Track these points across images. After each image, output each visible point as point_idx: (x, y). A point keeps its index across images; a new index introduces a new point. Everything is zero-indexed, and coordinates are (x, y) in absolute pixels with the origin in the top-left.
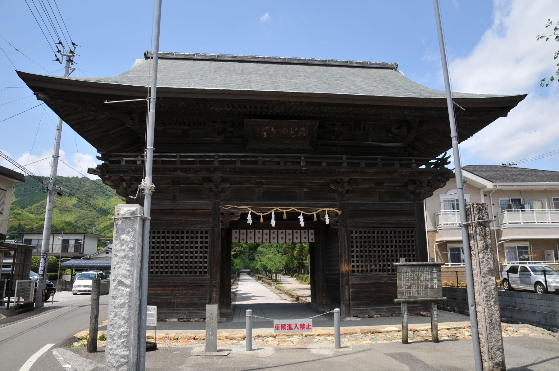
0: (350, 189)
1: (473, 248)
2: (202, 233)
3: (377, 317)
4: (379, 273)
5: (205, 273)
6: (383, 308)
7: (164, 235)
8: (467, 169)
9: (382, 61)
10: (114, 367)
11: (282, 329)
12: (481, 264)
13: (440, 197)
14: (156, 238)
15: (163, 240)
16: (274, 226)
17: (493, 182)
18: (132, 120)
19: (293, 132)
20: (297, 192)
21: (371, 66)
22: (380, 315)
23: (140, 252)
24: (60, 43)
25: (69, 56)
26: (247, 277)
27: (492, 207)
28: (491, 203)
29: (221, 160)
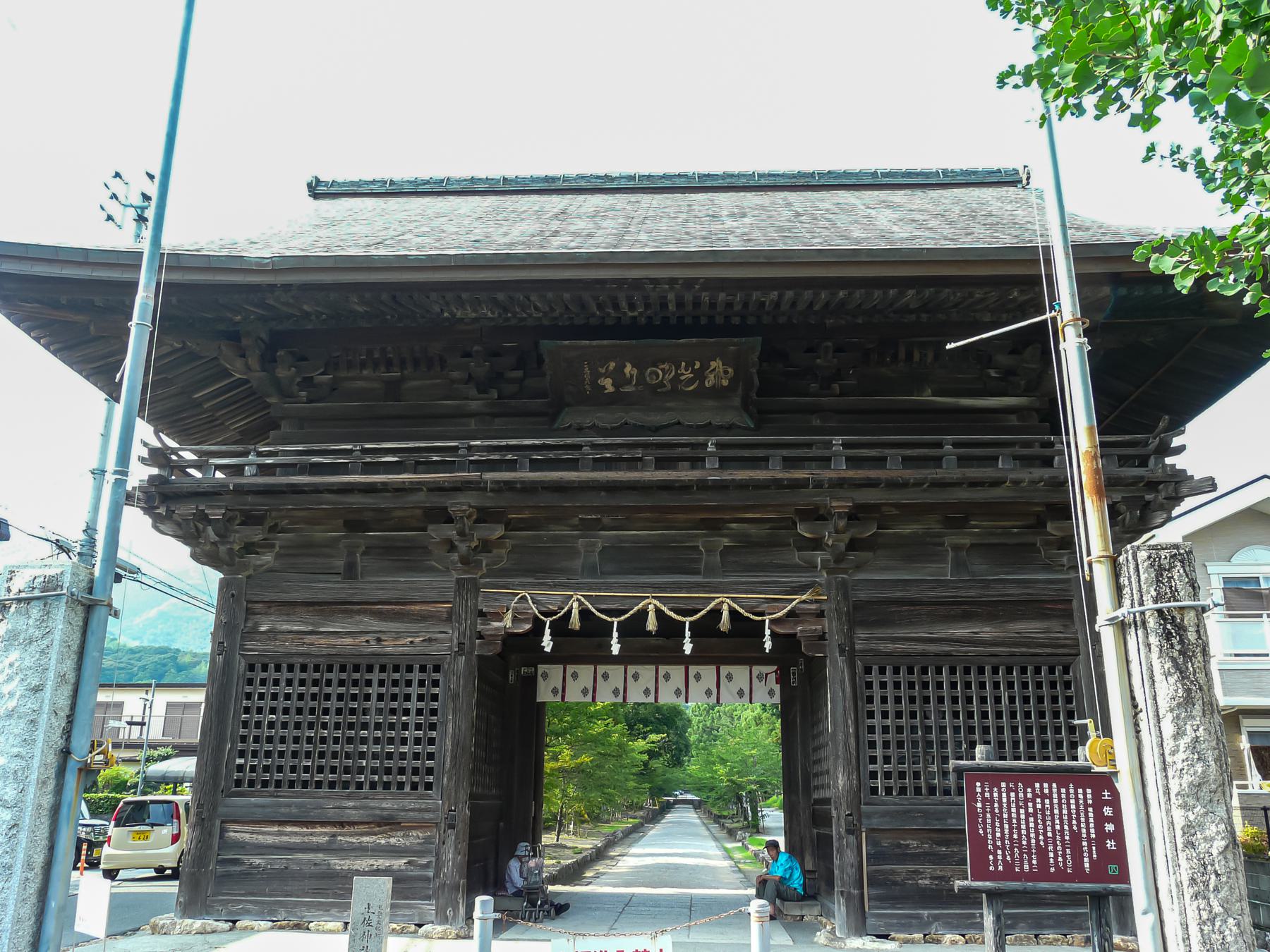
0: (858, 536)
2: (423, 669)
3: (954, 943)
5: (429, 786)
7: (317, 676)
12: (1169, 759)
13: (1210, 570)
14: (296, 683)
15: (315, 689)
16: (617, 653)
18: (243, 356)
21: (947, 180)
22: (963, 936)
23: (64, 701)
26: (691, 816)
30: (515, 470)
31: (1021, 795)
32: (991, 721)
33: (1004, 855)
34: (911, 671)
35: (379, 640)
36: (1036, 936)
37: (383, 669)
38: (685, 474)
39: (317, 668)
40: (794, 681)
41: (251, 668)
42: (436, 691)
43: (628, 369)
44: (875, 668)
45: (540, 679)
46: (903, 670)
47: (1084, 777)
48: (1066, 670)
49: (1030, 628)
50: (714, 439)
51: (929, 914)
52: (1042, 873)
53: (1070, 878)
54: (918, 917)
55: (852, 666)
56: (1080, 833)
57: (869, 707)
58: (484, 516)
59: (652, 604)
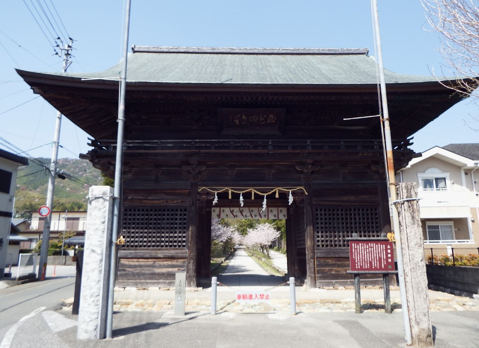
1: (402, 224)
3: (342, 289)
4: (344, 248)
5: (184, 246)
6: (348, 282)
8: (445, 148)
9: (353, 48)
10: (86, 322)
11: (243, 299)
17: (474, 160)
19: (263, 119)
20: (267, 173)
24: (59, 38)
25: (68, 51)
27: (474, 185)
28: (472, 182)
29: (197, 145)
30: (209, 149)
31: (365, 247)
32: (353, 225)
33: (360, 264)
34: (329, 210)
35: (167, 201)
36: (366, 287)
37: (181, 210)
38: (260, 151)
39: (147, 210)
40: (291, 213)
41: (126, 210)
42: (185, 217)
43: (244, 117)
44: (319, 210)
45: (212, 212)
46: (327, 210)
47: (386, 242)
48: (376, 210)
49: (366, 197)
50: (271, 140)
51: (335, 282)
52: (371, 268)
53: (378, 270)
54: (332, 282)
55: (312, 209)
56: (381, 257)
57: (317, 221)
58: (200, 163)
59: (253, 191)
